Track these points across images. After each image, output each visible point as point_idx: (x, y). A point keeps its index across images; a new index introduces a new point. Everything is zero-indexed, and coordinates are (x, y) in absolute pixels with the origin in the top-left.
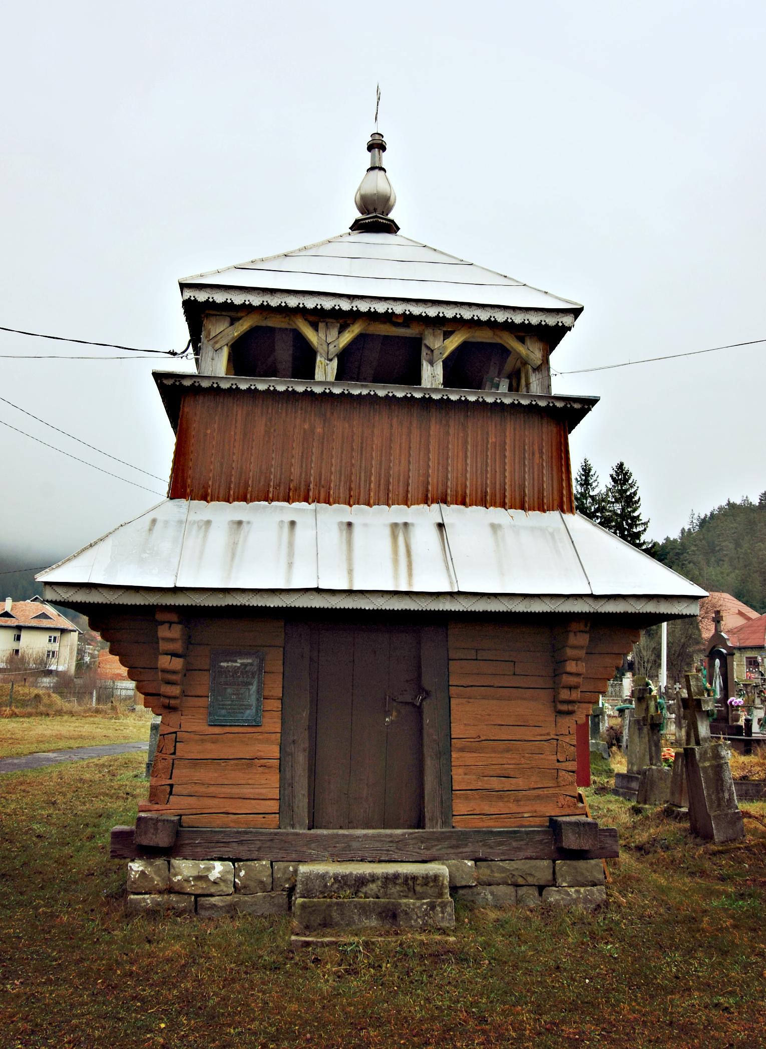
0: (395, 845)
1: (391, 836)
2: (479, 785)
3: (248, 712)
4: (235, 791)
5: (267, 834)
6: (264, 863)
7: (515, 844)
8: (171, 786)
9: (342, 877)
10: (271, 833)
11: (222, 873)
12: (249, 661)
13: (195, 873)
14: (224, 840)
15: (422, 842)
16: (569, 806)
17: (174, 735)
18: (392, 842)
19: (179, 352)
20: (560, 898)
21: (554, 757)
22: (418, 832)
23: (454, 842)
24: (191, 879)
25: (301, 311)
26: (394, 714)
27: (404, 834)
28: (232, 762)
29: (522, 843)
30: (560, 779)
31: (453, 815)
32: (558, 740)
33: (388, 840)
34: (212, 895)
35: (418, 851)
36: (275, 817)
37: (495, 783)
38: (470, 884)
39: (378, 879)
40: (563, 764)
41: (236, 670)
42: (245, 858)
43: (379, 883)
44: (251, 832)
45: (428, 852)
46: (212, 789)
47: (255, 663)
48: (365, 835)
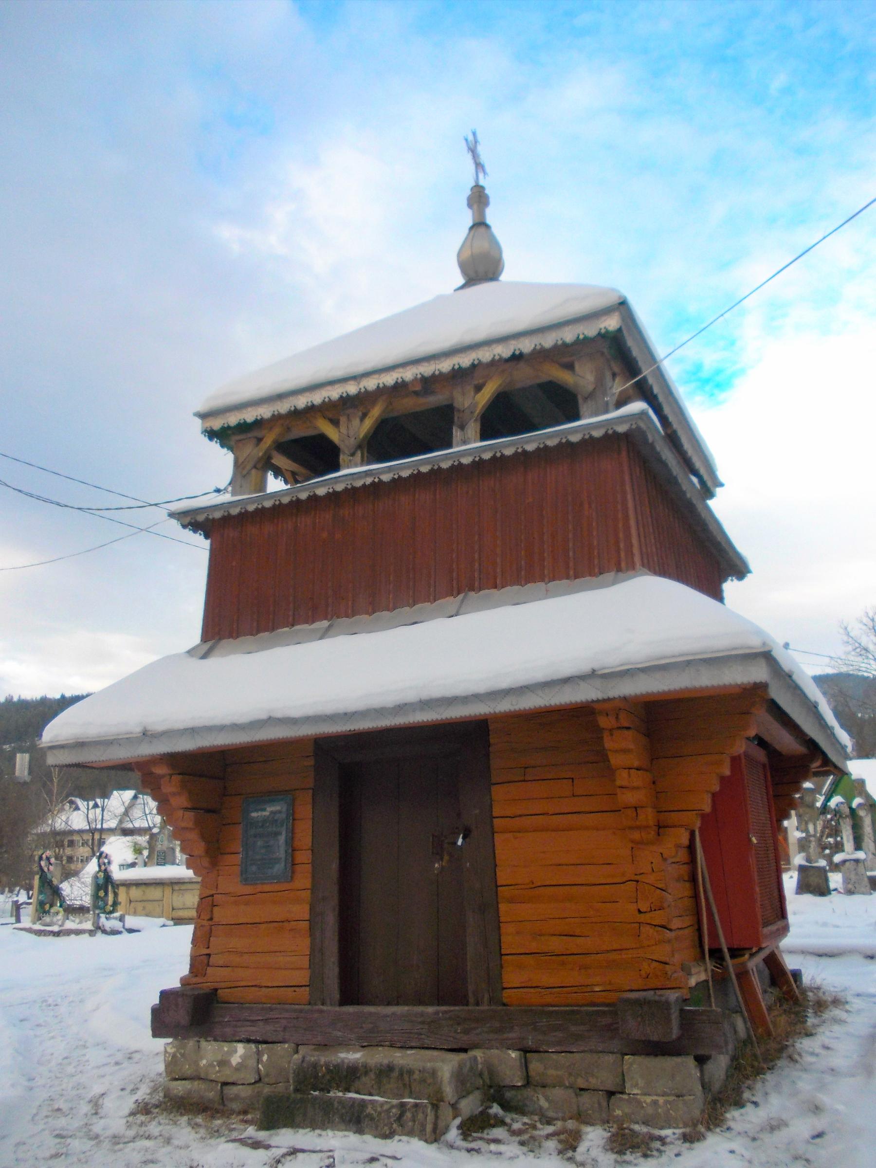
1: (422, 1014)
2: (534, 946)
6: (286, 1046)
7: (573, 1029)
8: (209, 955)
10: (295, 1011)
11: (244, 1057)
12: (278, 808)
13: (219, 1058)
14: (251, 1018)
15: (459, 1024)
16: (657, 976)
17: (210, 898)
18: (423, 1023)
19: (222, 488)
21: (633, 907)
23: (497, 1025)
24: (215, 1063)
25: (311, 409)
26: (446, 858)
27: (437, 1013)
28: (263, 926)
29: (582, 1028)
32: (637, 881)
36: (305, 991)
37: (555, 944)
39: (371, 1070)
40: (648, 915)
41: (265, 820)
44: (276, 1009)
45: (465, 1038)
47: (284, 810)
48: (393, 1014)
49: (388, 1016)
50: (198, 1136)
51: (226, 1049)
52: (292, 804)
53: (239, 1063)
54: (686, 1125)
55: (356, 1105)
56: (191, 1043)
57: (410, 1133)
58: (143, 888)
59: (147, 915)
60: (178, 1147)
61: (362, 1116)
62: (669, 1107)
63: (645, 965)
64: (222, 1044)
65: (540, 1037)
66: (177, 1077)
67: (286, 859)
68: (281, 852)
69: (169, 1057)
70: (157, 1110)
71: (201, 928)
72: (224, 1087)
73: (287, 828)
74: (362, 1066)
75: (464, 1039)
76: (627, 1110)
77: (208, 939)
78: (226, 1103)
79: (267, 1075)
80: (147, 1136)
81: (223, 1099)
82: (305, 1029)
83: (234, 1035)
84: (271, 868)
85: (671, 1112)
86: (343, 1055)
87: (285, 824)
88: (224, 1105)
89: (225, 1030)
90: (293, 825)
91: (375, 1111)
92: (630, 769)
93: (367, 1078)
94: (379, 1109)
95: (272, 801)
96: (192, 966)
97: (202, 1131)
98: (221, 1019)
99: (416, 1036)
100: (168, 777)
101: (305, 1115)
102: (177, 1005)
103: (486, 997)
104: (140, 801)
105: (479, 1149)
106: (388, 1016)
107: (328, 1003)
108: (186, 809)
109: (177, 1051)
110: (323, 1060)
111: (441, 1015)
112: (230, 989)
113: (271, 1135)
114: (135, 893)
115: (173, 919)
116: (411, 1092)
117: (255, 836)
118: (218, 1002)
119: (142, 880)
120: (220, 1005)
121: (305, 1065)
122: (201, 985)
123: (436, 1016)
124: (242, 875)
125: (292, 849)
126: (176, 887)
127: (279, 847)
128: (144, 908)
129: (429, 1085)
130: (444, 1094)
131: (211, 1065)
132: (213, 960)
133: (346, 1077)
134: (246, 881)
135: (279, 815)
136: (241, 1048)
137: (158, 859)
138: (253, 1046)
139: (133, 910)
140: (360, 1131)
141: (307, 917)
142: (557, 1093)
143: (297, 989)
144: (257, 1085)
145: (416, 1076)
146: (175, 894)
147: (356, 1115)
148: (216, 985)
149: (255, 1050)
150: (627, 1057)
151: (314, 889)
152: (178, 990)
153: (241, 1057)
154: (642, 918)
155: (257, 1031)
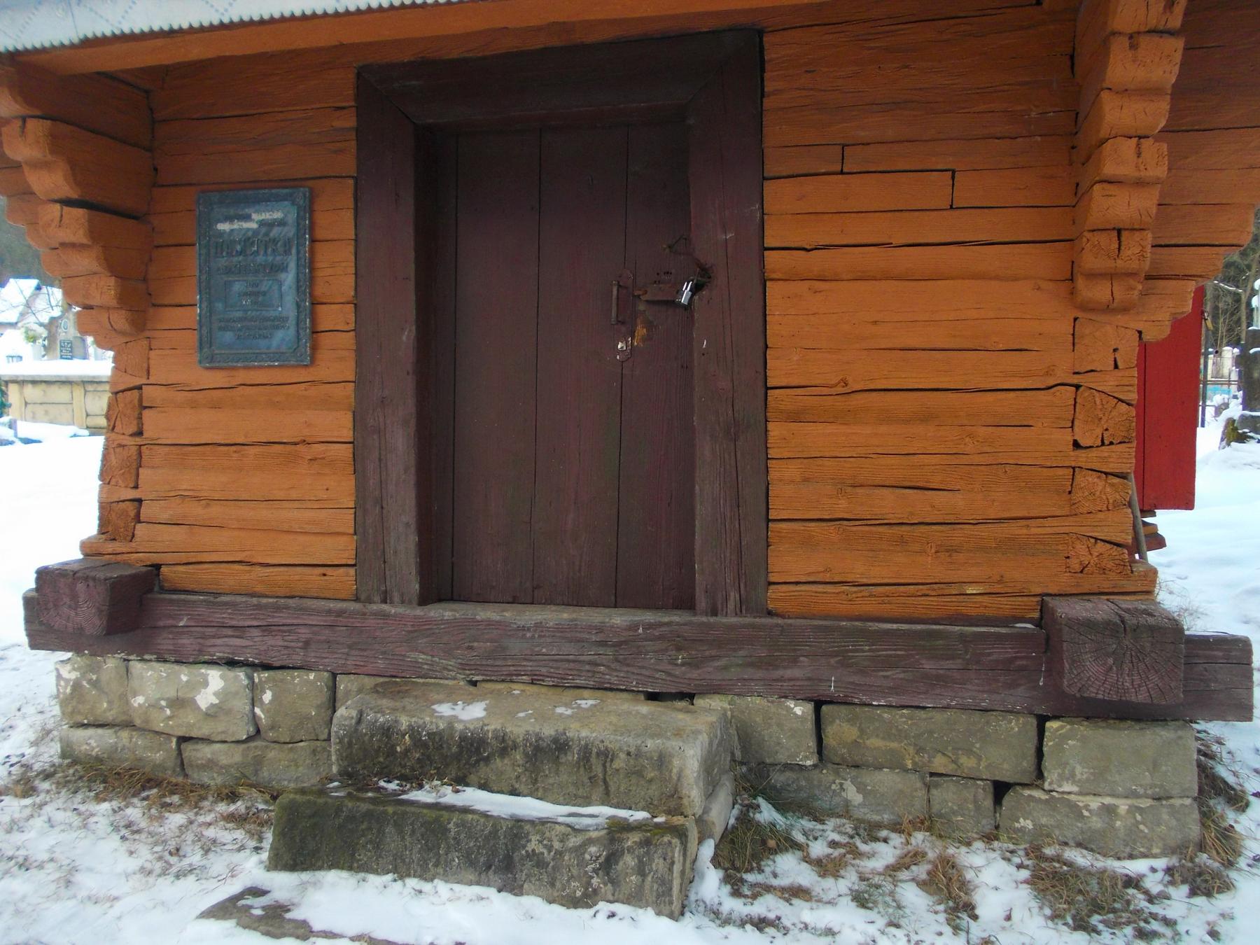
0: (610, 651)
2: (842, 507)
3: (279, 335)
4: (264, 513)
5: (318, 612)
6: (312, 676)
7: (928, 665)
9: (429, 734)
10: (329, 612)
11: (223, 695)
12: (278, 215)
13: (172, 693)
14: (234, 623)
17: (136, 392)
20: (1052, 822)
22: (669, 624)
24: (163, 703)
27: (633, 627)
28: (252, 451)
30: (1078, 495)
31: (770, 583)
33: (594, 638)
34: (207, 740)
35: (669, 667)
37: (888, 504)
38: (798, 761)
39: (515, 747)
40: (1093, 453)
42: (277, 664)
43: (518, 756)
45: (695, 674)
46: (216, 510)
47: (292, 217)
48: (538, 625)
49: (529, 629)
50: (133, 864)
51: (184, 678)
52: (309, 209)
53: (212, 705)
54: (1168, 851)
55: (501, 833)
56: (111, 663)
57: (635, 899)
58: (43, 386)
59: (51, 422)
60: (89, 898)
61: (516, 857)
62: (1139, 818)
63: (1081, 548)
64: (177, 667)
65: (856, 679)
66: (86, 722)
67: (298, 322)
68: (288, 308)
69: (66, 688)
70: (46, 785)
71: (118, 450)
72: (183, 746)
73: (298, 259)
74: (496, 737)
75: (687, 677)
76: (1044, 821)
77: (134, 472)
78: (189, 771)
79: (273, 728)
80: (21, 860)
81: (182, 764)
82: (350, 647)
83: (201, 652)
84: (266, 337)
85: (1142, 827)
86: (445, 709)
87: (294, 251)
88: (186, 776)
89: (181, 641)
90: (312, 252)
91: (550, 848)
92: (1140, 138)
93: (506, 761)
94: (557, 845)
95: (257, 201)
96: (104, 522)
97: (145, 854)
98: (170, 622)
99: (587, 667)
100: (20, 123)
101: (377, 846)
102: (74, 597)
103: (733, 596)
104: (44, 290)
105: (779, 918)
106: (529, 629)
107: (396, 598)
108: (67, 202)
109: (83, 675)
110: (404, 722)
111: (640, 631)
112: (185, 567)
113: (303, 886)
114: (30, 391)
115: (88, 428)
116: (607, 793)
117: (228, 271)
118: (163, 590)
119: (40, 376)
120: (167, 596)
121: (363, 729)
122: (125, 557)
123: (631, 633)
124: (201, 348)
125: (312, 302)
126: (90, 388)
127: (281, 296)
128: (47, 413)
129: (650, 781)
130: (685, 801)
131: (155, 706)
132: (145, 511)
133: (457, 758)
134: (211, 361)
135: (280, 229)
136: (216, 679)
137: (61, 351)
138: (241, 675)
139: (31, 415)
140: (513, 887)
141: (347, 434)
142: (886, 780)
143: (329, 571)
144: (252, 744)
145: (619, 763)
146: (90, 396)
147: (502, 852)
148: (156, 558)
149: (246, 682)
150: (1052, 725)
151: (361, 383)
152: (76, 567)
153: (215, 694)
154: (1082, 458)
155: (251, 646)
